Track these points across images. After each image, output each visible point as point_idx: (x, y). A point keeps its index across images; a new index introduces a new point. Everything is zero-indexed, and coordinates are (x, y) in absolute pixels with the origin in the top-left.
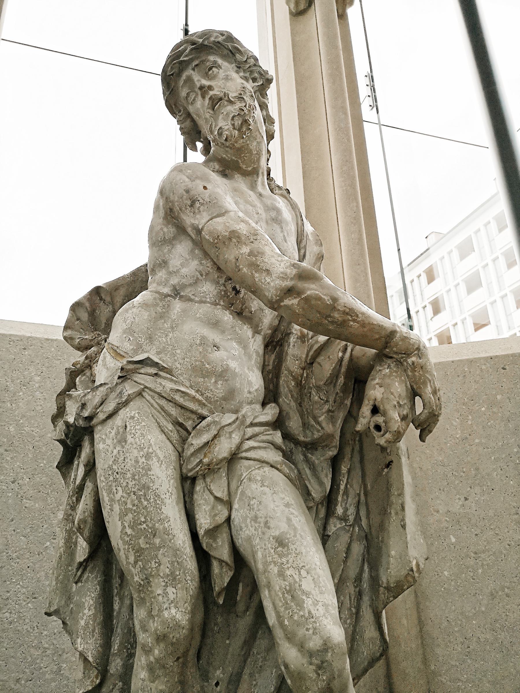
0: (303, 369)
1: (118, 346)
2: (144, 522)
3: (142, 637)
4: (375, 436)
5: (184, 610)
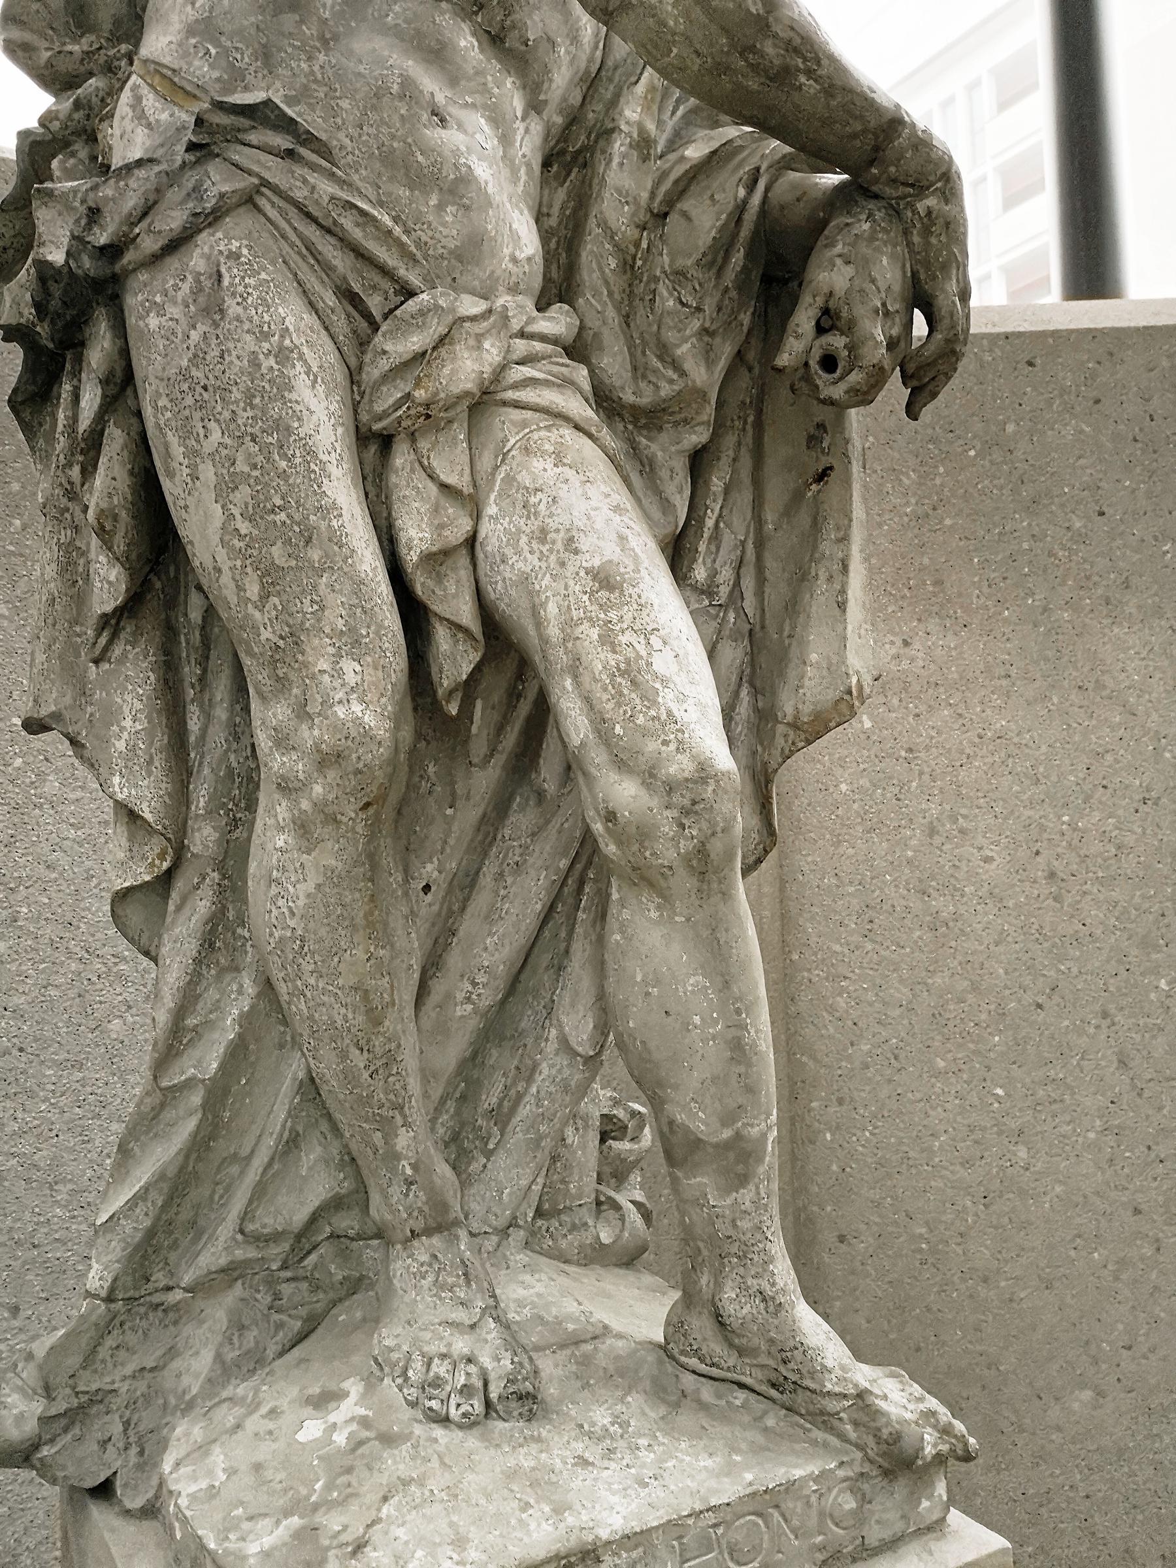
1: (176, 67)
3: (276, 763)
4: (818, 382)
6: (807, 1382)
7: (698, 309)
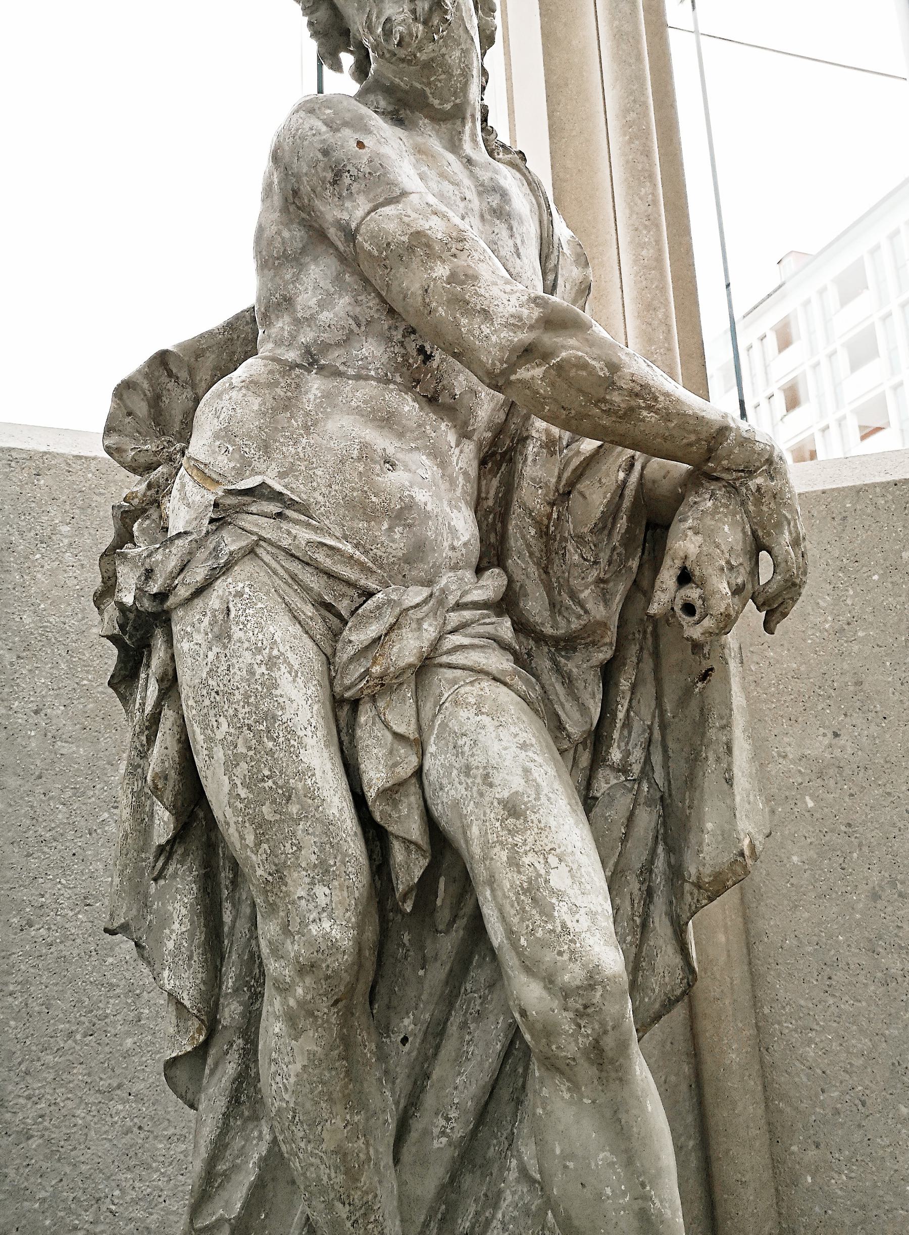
0: (552, 504)
1: (207, 462)
3: (273, 967)
4: (684, 623)
5: (344, 923)
7: (595, 563)
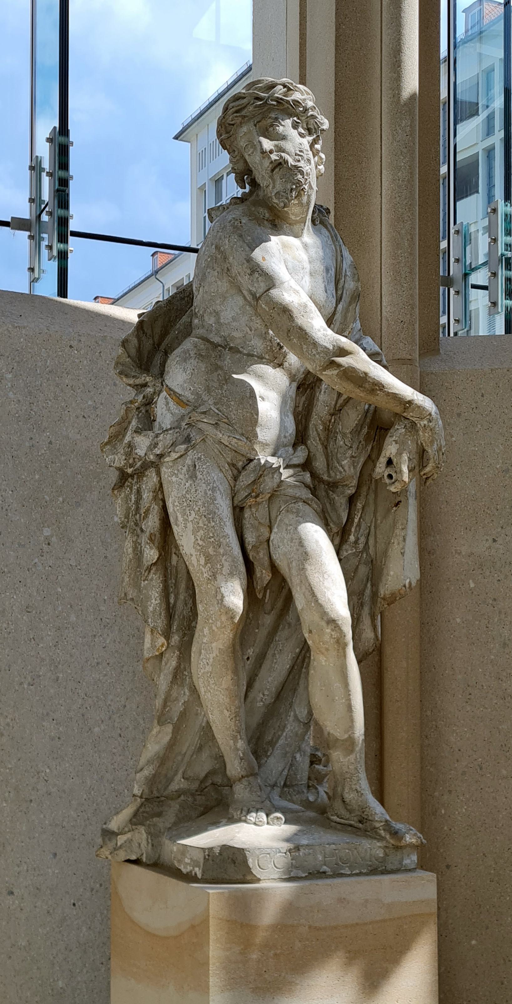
0: (332, 415)
2: (212, 537)
6: (370, 818)
7: (351, 447)
